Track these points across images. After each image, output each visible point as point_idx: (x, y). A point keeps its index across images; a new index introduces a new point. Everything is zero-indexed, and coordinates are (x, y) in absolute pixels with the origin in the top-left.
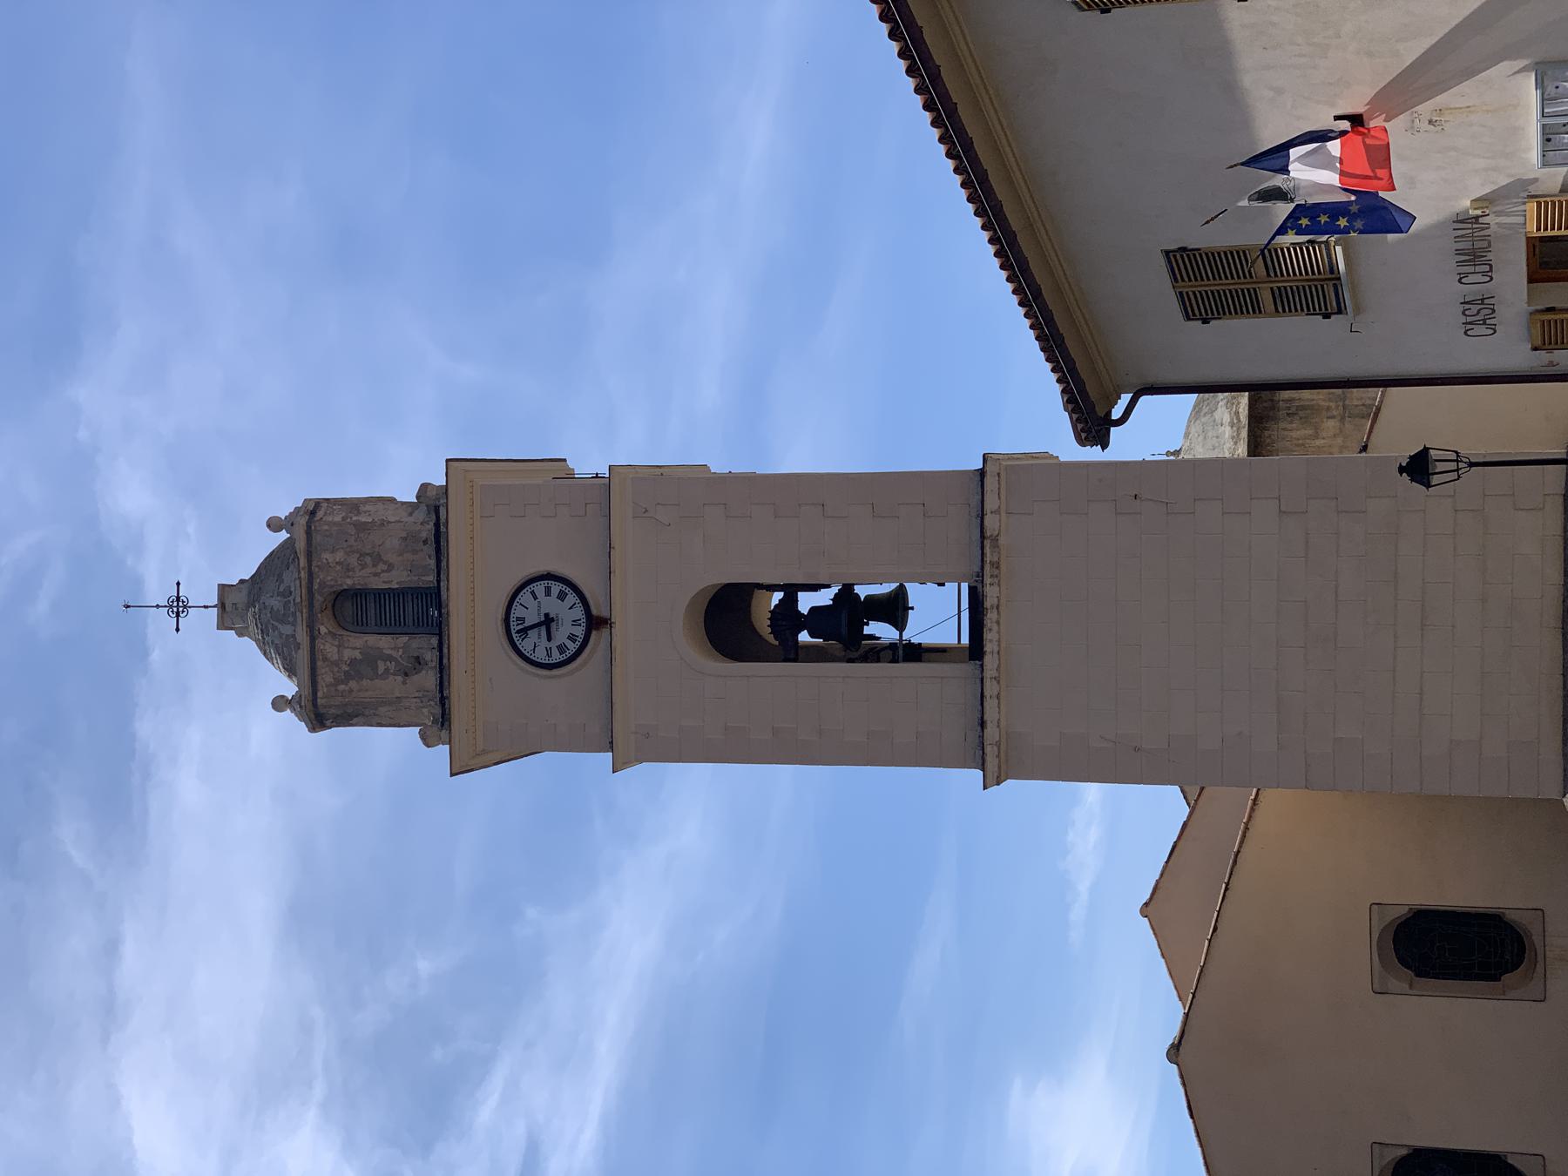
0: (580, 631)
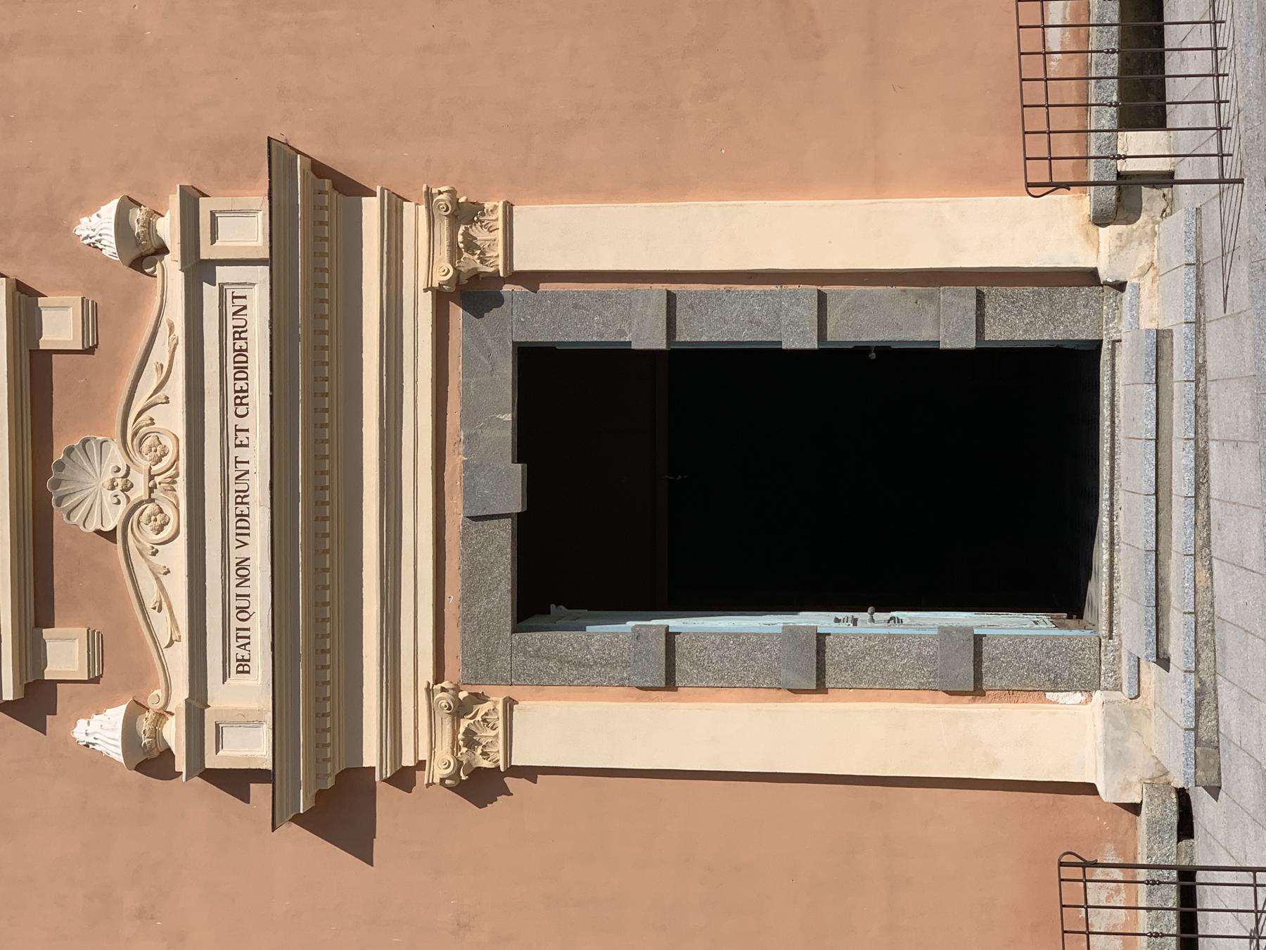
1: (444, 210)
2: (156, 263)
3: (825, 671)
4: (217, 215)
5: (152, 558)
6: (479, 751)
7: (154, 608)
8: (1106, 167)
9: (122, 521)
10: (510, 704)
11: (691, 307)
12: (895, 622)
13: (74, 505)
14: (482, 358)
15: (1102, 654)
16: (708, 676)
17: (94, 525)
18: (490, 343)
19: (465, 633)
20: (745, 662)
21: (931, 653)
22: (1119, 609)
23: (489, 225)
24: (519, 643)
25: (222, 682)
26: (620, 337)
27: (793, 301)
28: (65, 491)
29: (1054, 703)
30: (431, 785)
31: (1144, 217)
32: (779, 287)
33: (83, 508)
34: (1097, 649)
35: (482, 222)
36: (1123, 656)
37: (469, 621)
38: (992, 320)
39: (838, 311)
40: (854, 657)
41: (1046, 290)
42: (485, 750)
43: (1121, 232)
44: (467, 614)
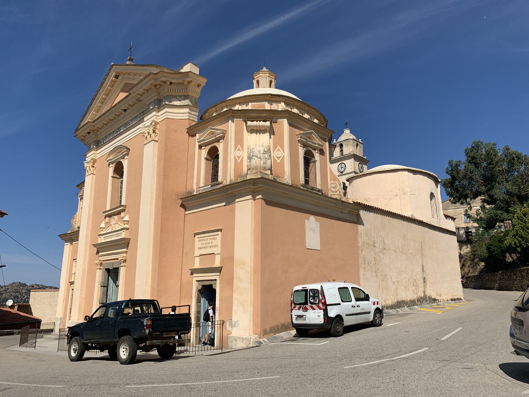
0: (341, 171)
10: (100, 269)
17: (111, 221)
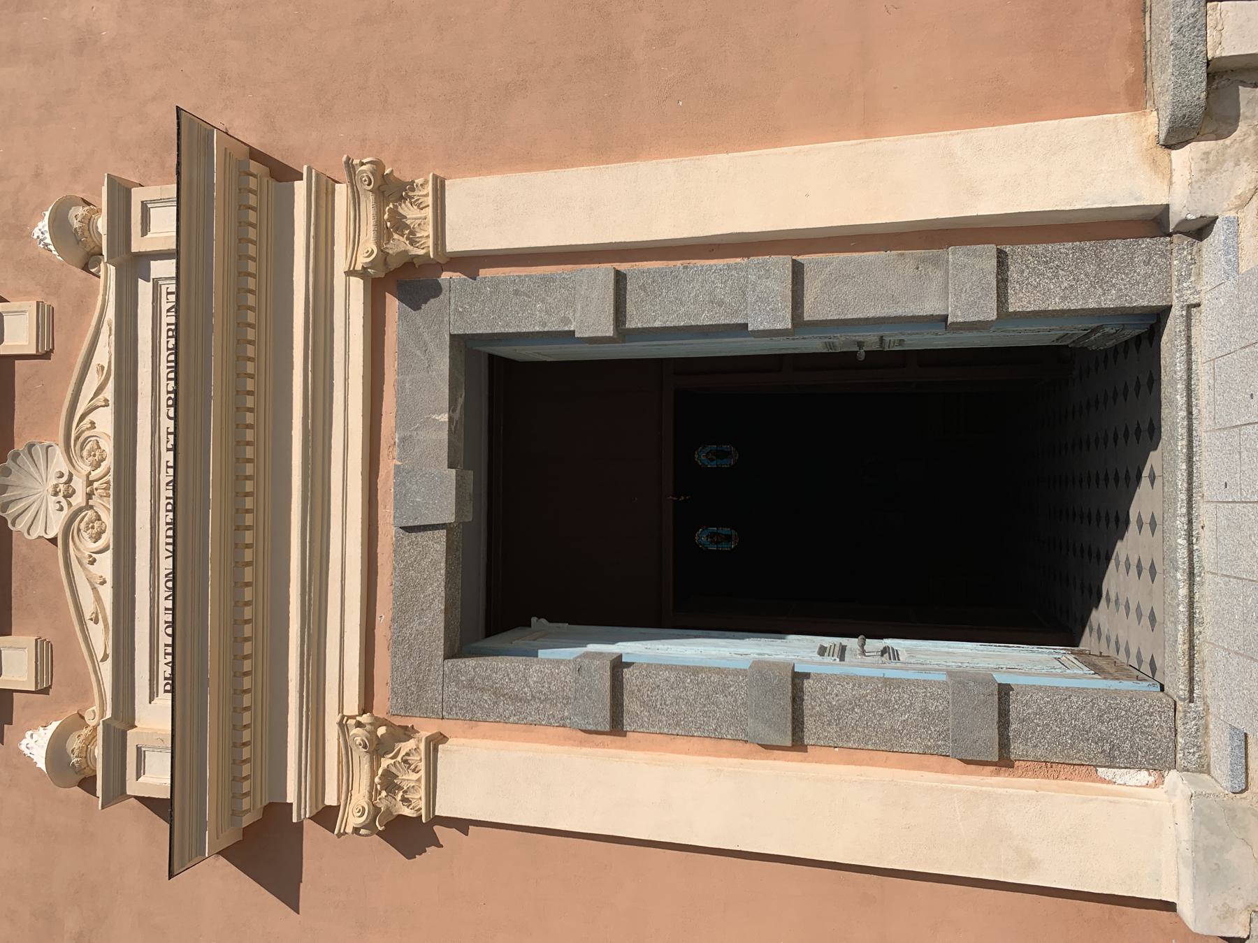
1: (367, 183)
2: (100, 264)
3: (803, 723)
4: (149, 206)
5: (90, 567)
6: (399, 797)
7: (91, 619)
8: (1191, 55)
9: (62, 528)
10: (435, 742)
11: (643, 288)
12: (890, 659)
13: (20, 512)
14: (418, 353)
15: (1179, 722)
16: (661, 721)
17: (37, 531)
18: (426, 337)
19: (395, 657)
20: (705, 706)
21: (940, 708)
22: (1204, 662)
23: (420, 201)
24: (451, 672)
25: (148, 702)
26: (564, 326)
27: (761, 273)
28: (14, 495)
29: (1109, 782)
30: (342, 834)
31: (1242, 127)
32: (746, 259)
33: (29, 514)
34: (1171, 714)
35: (411, 198)
36: (1211, 726)
37: (400, 644)
38: (1017, 287)
39: (818, 283)
40: (840, 708)
41: (1091, 245)
42: (406, 796)
43: (1208, 150)
44: (398, 636)
